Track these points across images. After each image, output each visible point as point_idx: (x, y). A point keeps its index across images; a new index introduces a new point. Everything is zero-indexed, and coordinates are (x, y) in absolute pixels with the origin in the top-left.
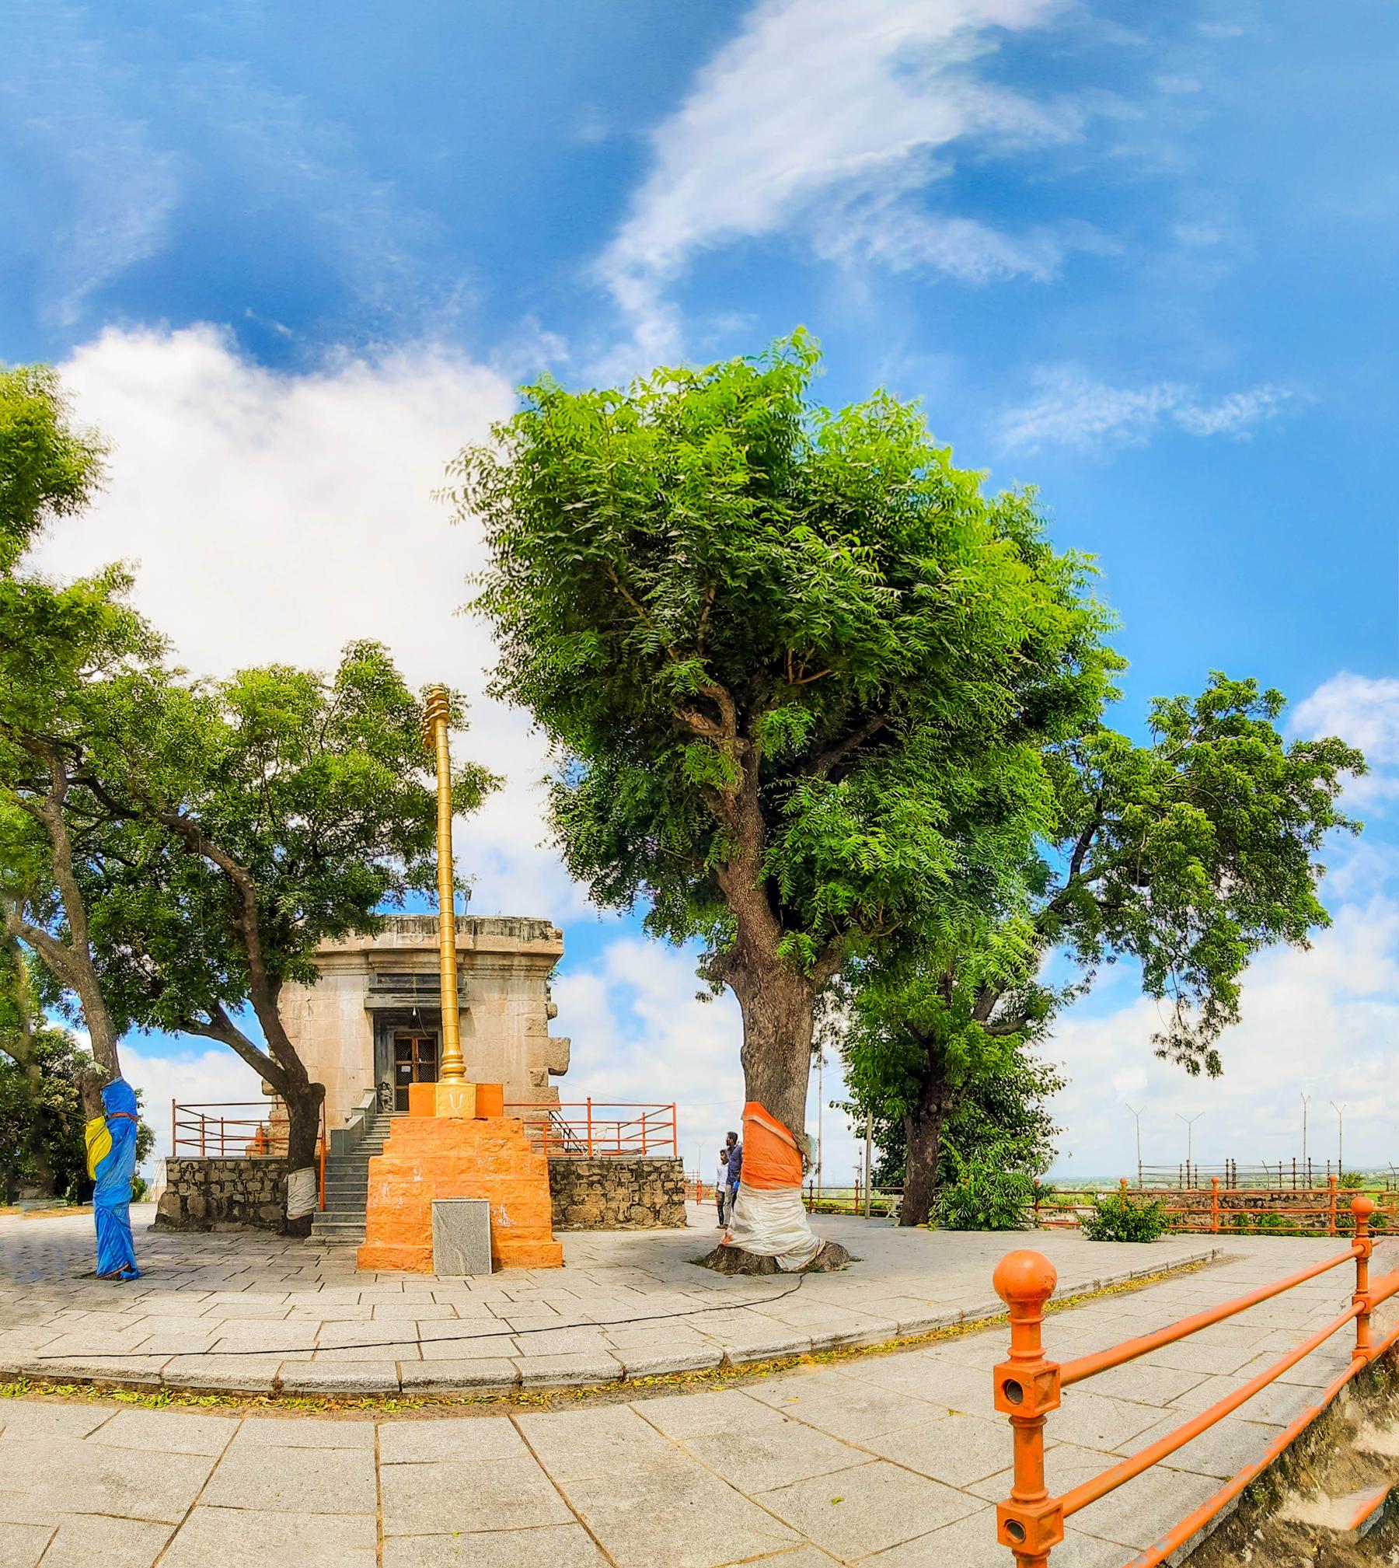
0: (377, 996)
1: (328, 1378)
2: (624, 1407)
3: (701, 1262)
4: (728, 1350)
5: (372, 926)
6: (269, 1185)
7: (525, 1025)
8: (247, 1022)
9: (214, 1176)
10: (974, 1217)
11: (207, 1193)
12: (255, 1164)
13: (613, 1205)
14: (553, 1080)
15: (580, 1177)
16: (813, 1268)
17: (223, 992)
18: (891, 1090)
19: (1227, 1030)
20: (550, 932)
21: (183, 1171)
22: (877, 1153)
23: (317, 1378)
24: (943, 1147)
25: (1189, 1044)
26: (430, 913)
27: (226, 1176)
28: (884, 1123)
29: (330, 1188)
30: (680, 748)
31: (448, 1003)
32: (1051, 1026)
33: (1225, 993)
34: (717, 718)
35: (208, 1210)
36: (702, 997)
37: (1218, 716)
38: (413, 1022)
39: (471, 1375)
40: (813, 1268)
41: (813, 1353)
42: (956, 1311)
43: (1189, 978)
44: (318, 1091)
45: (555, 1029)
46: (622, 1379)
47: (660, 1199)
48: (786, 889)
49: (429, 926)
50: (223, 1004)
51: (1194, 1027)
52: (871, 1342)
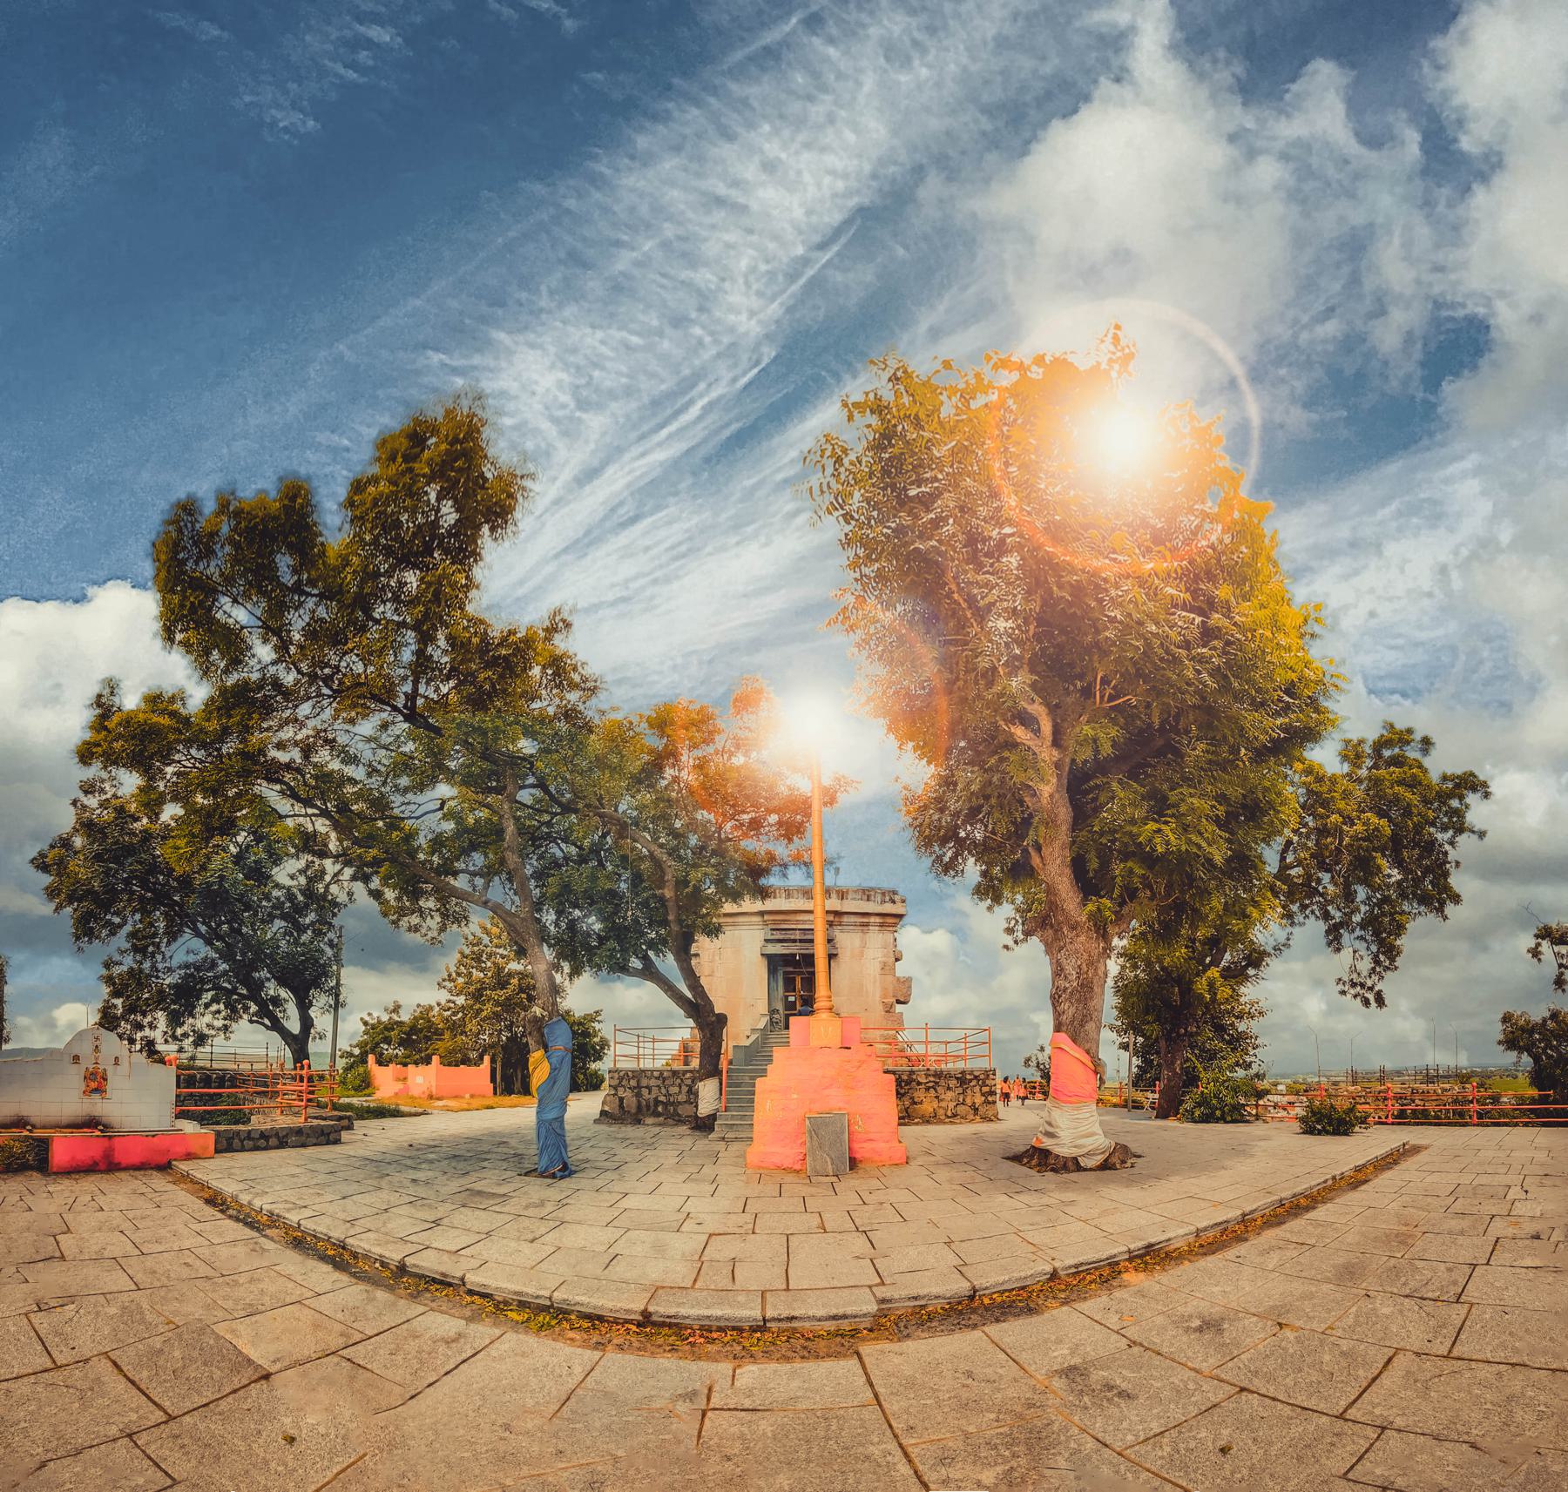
0: (770, 945)
1: (694, 1312)
2: (977, 1334)
3: (1016, 1158)
4: (1057, 1264)
5: (764, 893)
6: (685, 1089)
7: (878, 967)
8: (667, 963)
9: (644, 1082)
10: (1213, 1113)
11: (639, 1095)
12: (675, 1073)
13: (943, 1104)
14: (899, 1008)
15: (919, 1084)
16: (1105, 1166)
17: (652, 945)
18: (1150, 1018)
19: (1388, 975)
20: (897, 898)
21: (621, 1079)
22: (1136, 1061)
23: (683, 1311)
24: (1188, 1060)
25: (1362, 985)
26: (807, 883)
27: (653, 1082)
28: (1140, 1040)
29: (731, 1093)
30: (1006, 754)
31: (820, 951)
32: (1265, 972)
33: (1392, 952)
34: (1037, 732)
35: (639, 1107)
36: (1006, 947)
37: (1387, 753)
38: (797, 964)
39: (834, 1311)
40: (1105, 1166)
41: (1130, 1260)
42: (1239, 1212)
43: (1361, 938)
44: (722, 1020)
45: (901, 969)
46: (972, 1298)
47: (979, 1100)
48: (1094, 864)
49: (807, 893)
50: (651, 953)
51: (1365, 973)
52: (1177, 1245)
